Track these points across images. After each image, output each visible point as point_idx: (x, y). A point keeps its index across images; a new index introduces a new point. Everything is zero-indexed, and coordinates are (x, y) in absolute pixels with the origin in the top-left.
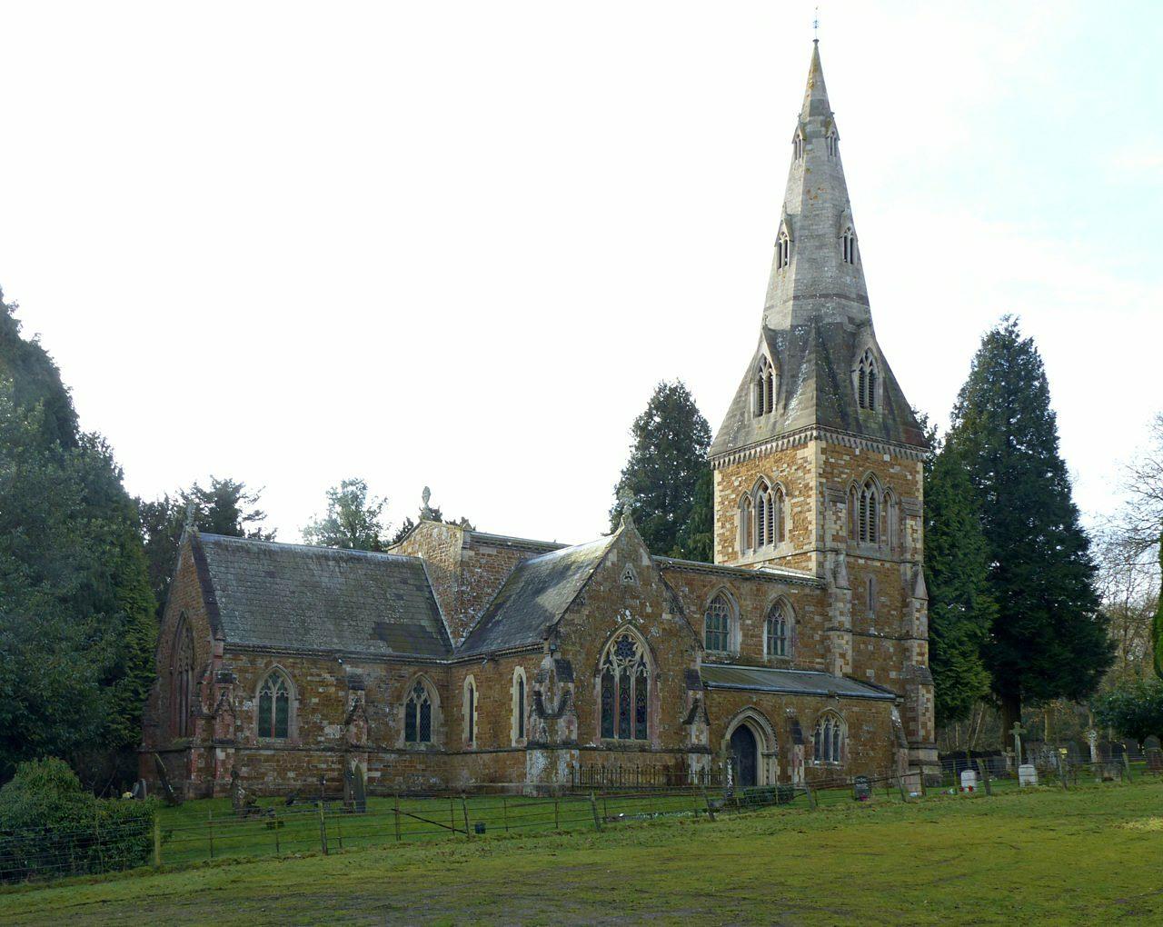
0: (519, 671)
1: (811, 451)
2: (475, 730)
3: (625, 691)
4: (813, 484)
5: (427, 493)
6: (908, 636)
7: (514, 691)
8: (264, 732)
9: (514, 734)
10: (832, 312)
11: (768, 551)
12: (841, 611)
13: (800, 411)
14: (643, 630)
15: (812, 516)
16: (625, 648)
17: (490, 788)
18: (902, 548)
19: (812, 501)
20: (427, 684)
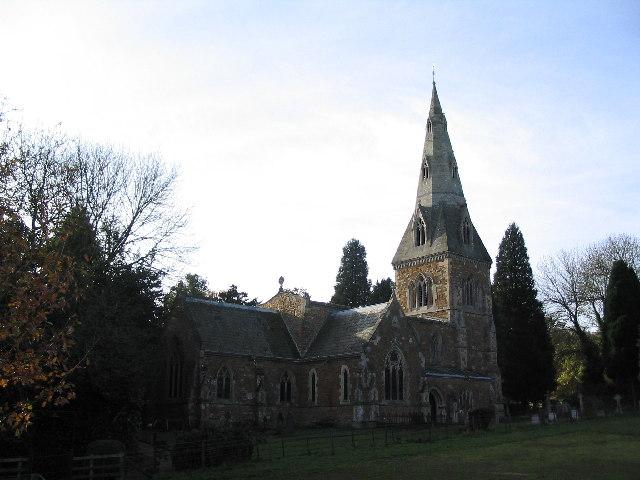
0: (344, 367)
1: (446, 263)
2: (316, 395)
3: (394, 375)
4: (447, 278)
5: (281, 280)
6: (489, 350)
7: (342, 377)
8: (219, 396)
9: (341, 397)
10: (450, 201)
11: (424, 309)
12: (462, 339)
13: (439, 245)
14: (402, 349)
15: (447, 293)
16: (394, 357)
17: (326, 425)
18: (484, 308)
19: (447, 286)
20: (290, 373)
